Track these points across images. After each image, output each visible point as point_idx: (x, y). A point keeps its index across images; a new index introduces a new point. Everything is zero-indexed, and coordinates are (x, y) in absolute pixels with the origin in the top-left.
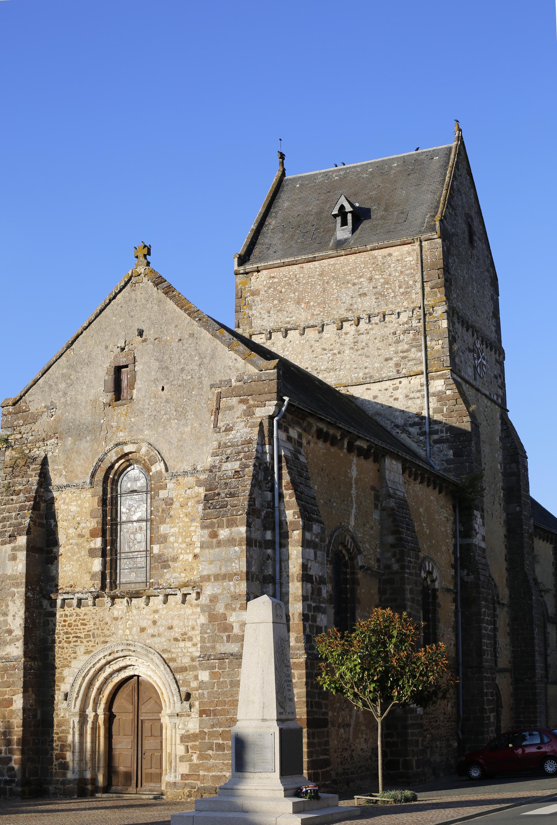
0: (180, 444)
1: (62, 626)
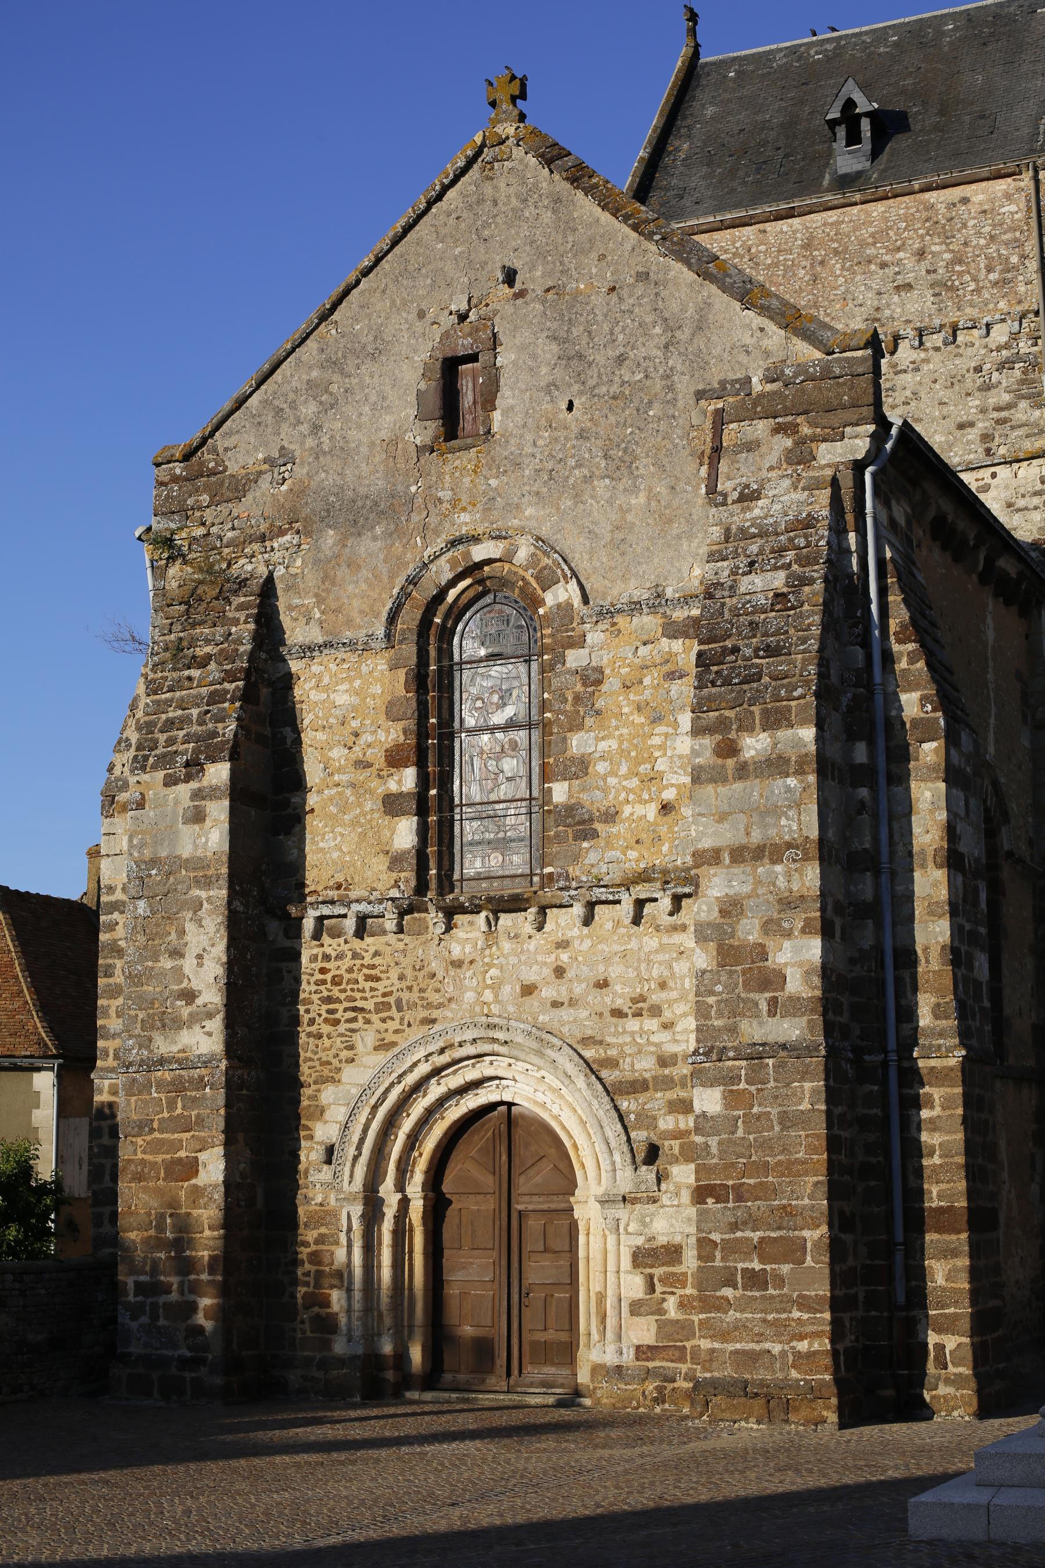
0: (620, 536)
1: (316, 984)
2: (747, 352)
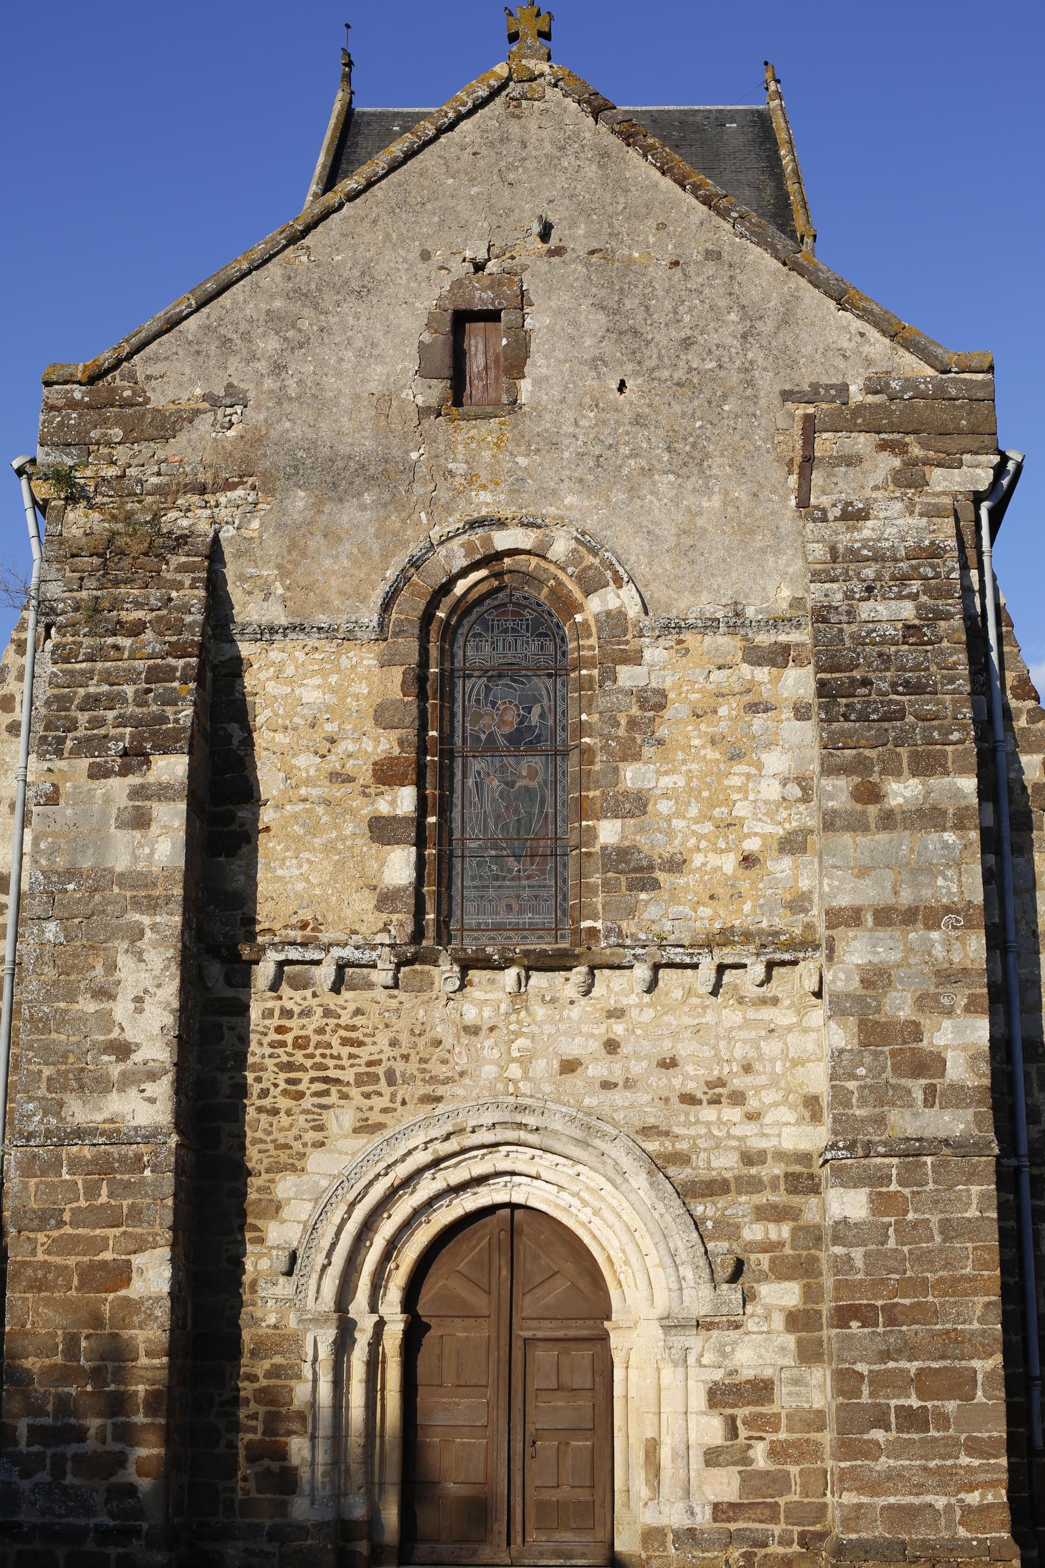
2: (844, 356)
